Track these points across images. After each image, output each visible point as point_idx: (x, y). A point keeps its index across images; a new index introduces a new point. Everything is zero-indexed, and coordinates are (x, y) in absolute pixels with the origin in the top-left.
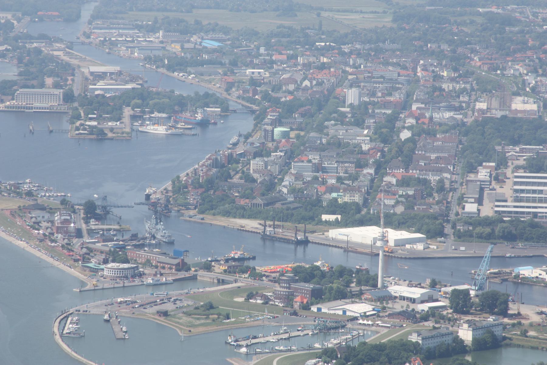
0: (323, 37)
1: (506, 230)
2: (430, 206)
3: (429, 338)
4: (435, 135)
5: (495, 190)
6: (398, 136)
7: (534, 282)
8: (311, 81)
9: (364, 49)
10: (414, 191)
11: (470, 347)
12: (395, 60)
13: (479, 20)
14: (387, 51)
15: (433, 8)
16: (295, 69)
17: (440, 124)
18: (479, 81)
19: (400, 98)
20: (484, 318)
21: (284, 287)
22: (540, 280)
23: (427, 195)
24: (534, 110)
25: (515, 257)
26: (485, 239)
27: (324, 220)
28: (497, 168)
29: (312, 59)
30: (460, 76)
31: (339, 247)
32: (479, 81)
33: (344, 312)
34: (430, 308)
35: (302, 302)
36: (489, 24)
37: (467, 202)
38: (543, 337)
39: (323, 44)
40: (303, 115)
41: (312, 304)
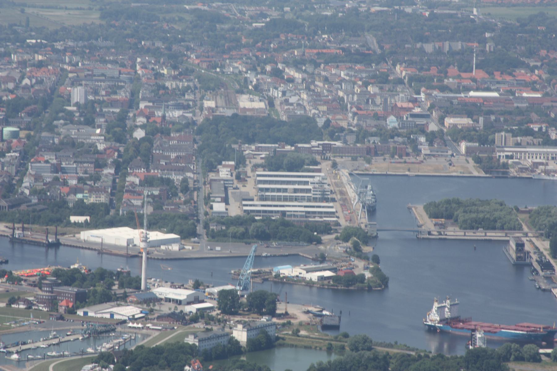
0: (33, 33)
1: (260, 230)
2: (178, 205)
3: (205, 340)
4: (169, 134)
5: (238, 189)
6: (131, 136)
7: (295, 281)
8: (30, 78)
9: (77, 46)
10: (160, 191)
11: (244, 348)
12: (111, 58)
13: (188, 17)
14: (101, 48)
15: (139, 5)
16: (10, 67)
17: (173, 123)
18: (200, 78)
19: (126, 97)
20: (253, 318)
21: (46, 291)
22: (300, 279)
23: (172, 194)
24: (263, 108)
25: (271, 256)
26: (239, 238)
27: (72, 221)
28: (236, 167)
29: (26, 57)
30: (180, 74)
31: (92, 249)
32: (200, 78)
33: (112, 315)
34: (198, 310)
35: (68, 307)
36: (198, 22)
37: (214, 201)
38: (314, 336)
39: (34, 41)
40: (29, 114)
41: (78, 308)
